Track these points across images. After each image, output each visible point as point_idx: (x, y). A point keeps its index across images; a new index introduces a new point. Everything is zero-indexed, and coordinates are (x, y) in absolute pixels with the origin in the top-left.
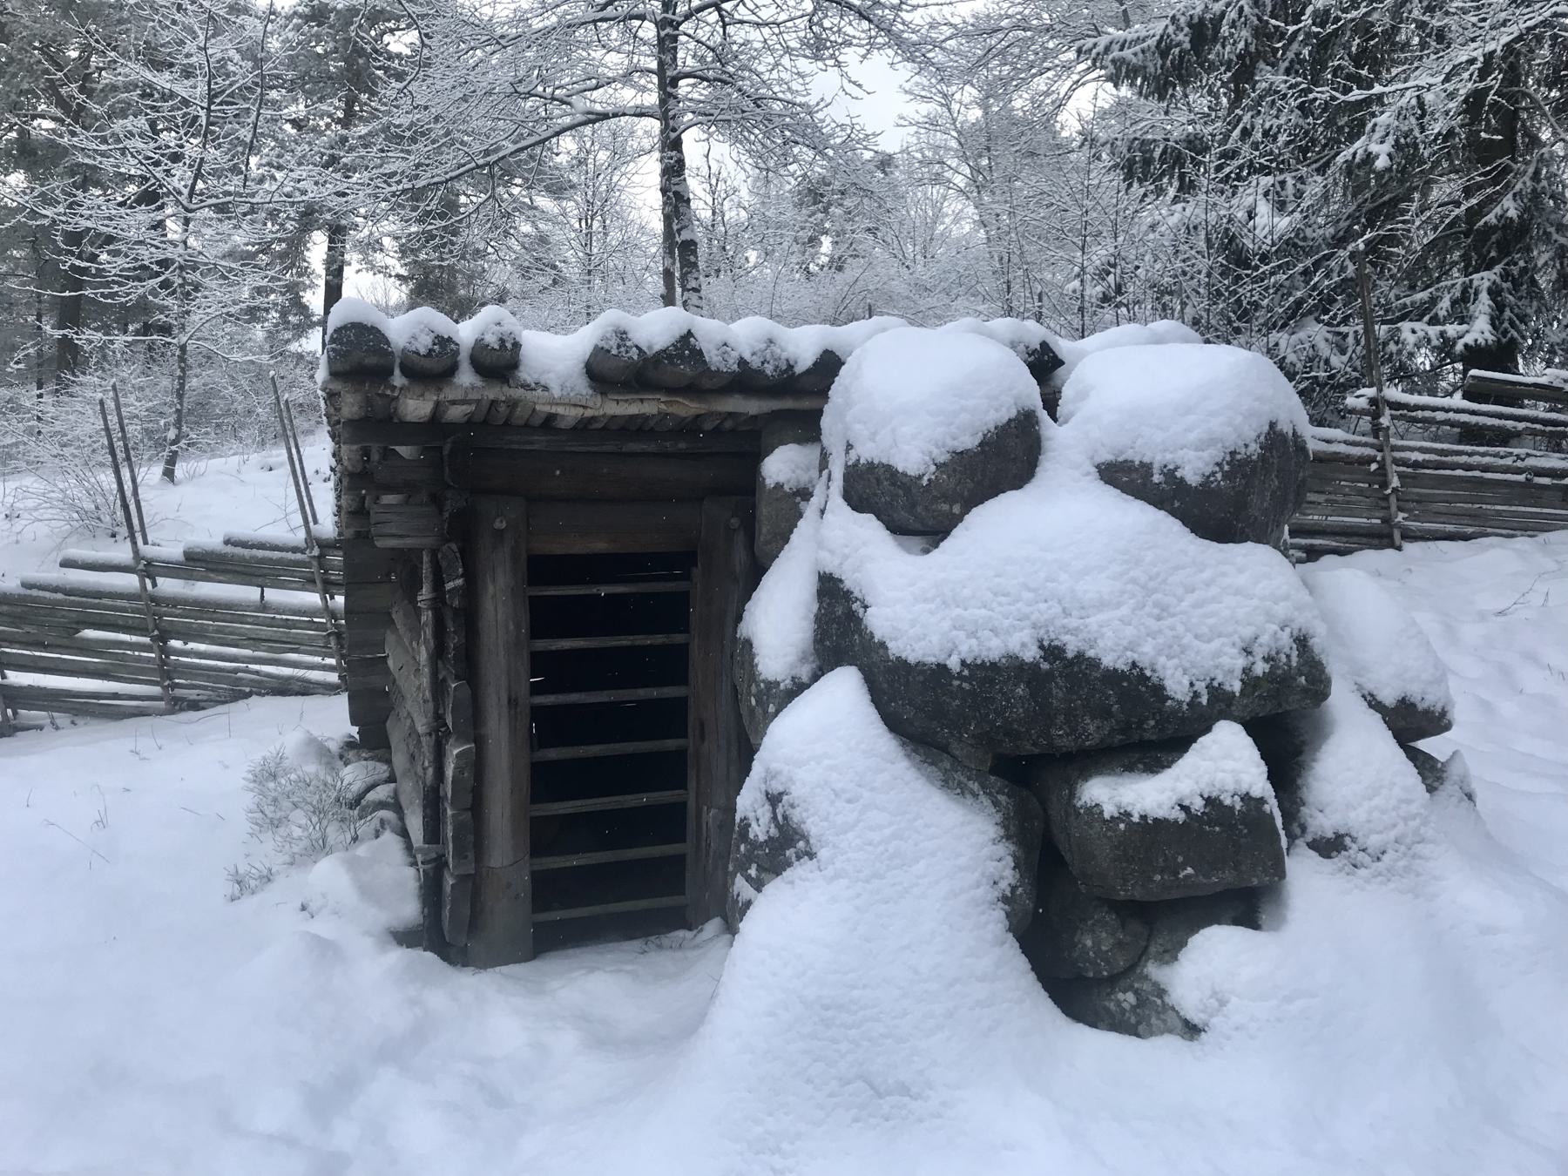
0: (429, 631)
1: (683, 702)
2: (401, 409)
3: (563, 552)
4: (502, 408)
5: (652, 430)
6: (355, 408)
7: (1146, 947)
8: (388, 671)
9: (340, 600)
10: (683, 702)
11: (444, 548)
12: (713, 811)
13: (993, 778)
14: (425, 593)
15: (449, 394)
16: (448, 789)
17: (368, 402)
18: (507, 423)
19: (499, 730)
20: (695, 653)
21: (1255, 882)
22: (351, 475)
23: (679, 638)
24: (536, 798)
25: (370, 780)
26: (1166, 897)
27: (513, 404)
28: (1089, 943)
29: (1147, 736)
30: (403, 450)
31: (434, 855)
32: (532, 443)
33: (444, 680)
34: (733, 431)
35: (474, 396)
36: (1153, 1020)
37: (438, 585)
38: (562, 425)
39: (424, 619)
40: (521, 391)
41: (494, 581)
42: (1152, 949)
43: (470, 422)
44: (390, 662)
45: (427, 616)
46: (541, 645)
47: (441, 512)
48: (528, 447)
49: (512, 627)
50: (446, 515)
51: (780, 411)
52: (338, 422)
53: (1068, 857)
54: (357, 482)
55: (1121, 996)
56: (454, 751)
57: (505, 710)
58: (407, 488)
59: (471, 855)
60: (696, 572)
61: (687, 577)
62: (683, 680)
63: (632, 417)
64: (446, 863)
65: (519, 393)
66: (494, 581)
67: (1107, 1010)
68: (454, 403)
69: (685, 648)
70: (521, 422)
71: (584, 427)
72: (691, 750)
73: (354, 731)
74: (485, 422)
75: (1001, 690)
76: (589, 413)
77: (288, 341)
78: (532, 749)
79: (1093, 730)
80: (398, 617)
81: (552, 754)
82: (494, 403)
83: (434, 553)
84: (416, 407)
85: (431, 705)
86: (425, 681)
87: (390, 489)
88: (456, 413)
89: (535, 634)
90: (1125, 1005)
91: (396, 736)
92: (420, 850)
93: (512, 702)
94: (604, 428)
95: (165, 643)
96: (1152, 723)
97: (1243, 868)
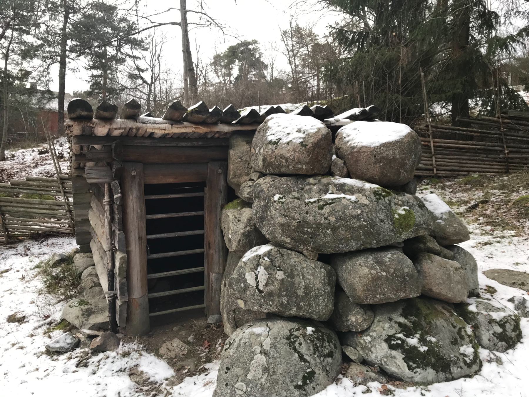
0: (108, 213)
1: (202, 236)
2: (96, 132)
3: (158, 183)
4: (134, 131)
5: (189, 138)
6: (79, 131)
7: (374, 320)
8: (90, 225)
9: (71, 200)
10: (202, 236)
11: (113, 182)
12: (214, 274)
13: (319, 262)
14: (106, 199)
15: (114, 126)
16: (117, 270)
17: (83, 130)
18: (136, 136)
19: (135, 248)
20: (207, 218)
21: (411, 296)
22: (76, 155)
23: (200, 213)
24: (149, 272)
25: (85, 266)
26: (381, 303)
27: (138, 129)
28: (354, 320)
29: (373, 246)
30: (97, 146)
31: (112, 294)
32: (145, 143)
33: (114, 230)
34: (218, 138)
35: (123, 126)
36: (377, 346)
37: (111, 196)
38: (156, 136)
39: (106, 209)
40: (141, 124)
41: (132, 194)
42: (376, 321)
43: (121, 136)
44: (91, 222)
45: (107, 208)
46: (150, 217)
47: (111, 169)
48: (143, 145)
49: (139, 211)
50: (114, 170)
51: (239, 131)
52: (72, 136)
53: (345, 289)
54: (79, 159)
55: (365, 338)
56: (119, 256)
57: (137, 241)
58: (97, 161)
59: (126, 294)
60: (206, 189)
61: (202, 191)
62: (202, 227)
63: (182, 133)
64: (117, 297)
65: (140, 125)
66: (132, 194)
67: (360, 342)
68: (116, 129)
69: (202, 217)
70: (141, 135)
71: (164, 137)
72: (205, 253)
73: (78, 247)
74: (127, 136)
75: (322, 231)
76: (167, 132)
77: (45, 104)
78: (148, 255)
79: (354, 245)
80: (93, 205)
81: (155, 256)
82: (131, 129)
83: (109, 185)
84: (101, 130)
85: (109, 240)
86: (107, 231)
87: (90, 160)
88: (116, 133)
89: (148, 212)
90: (367, 341)
91: (94, 247)
92: (107, 293)
93: (140, 238)
94: (171, 137)
95: (4, 216)
96: (375, 242)
97: (407, 292)
